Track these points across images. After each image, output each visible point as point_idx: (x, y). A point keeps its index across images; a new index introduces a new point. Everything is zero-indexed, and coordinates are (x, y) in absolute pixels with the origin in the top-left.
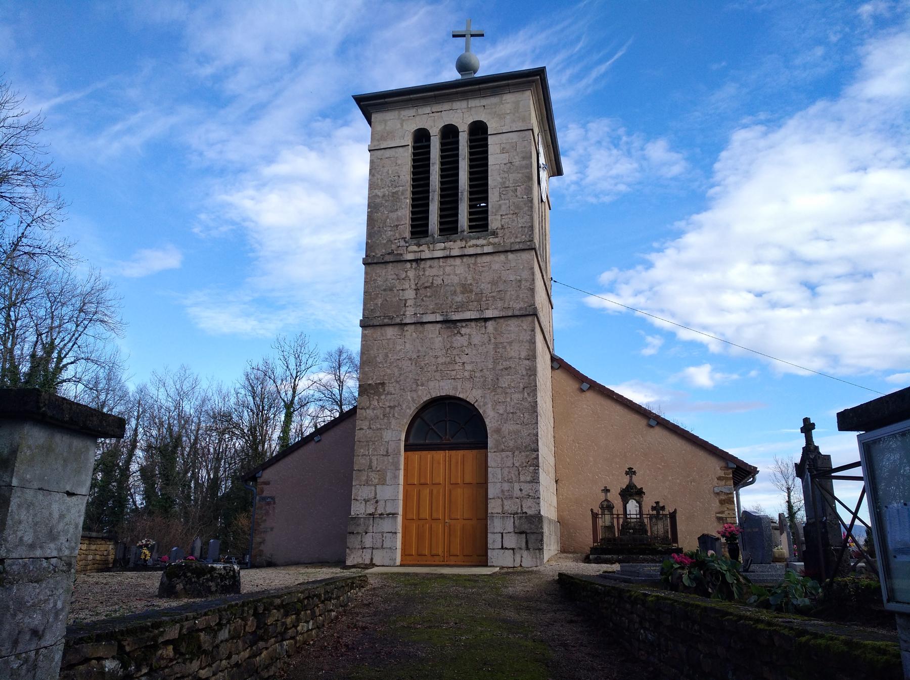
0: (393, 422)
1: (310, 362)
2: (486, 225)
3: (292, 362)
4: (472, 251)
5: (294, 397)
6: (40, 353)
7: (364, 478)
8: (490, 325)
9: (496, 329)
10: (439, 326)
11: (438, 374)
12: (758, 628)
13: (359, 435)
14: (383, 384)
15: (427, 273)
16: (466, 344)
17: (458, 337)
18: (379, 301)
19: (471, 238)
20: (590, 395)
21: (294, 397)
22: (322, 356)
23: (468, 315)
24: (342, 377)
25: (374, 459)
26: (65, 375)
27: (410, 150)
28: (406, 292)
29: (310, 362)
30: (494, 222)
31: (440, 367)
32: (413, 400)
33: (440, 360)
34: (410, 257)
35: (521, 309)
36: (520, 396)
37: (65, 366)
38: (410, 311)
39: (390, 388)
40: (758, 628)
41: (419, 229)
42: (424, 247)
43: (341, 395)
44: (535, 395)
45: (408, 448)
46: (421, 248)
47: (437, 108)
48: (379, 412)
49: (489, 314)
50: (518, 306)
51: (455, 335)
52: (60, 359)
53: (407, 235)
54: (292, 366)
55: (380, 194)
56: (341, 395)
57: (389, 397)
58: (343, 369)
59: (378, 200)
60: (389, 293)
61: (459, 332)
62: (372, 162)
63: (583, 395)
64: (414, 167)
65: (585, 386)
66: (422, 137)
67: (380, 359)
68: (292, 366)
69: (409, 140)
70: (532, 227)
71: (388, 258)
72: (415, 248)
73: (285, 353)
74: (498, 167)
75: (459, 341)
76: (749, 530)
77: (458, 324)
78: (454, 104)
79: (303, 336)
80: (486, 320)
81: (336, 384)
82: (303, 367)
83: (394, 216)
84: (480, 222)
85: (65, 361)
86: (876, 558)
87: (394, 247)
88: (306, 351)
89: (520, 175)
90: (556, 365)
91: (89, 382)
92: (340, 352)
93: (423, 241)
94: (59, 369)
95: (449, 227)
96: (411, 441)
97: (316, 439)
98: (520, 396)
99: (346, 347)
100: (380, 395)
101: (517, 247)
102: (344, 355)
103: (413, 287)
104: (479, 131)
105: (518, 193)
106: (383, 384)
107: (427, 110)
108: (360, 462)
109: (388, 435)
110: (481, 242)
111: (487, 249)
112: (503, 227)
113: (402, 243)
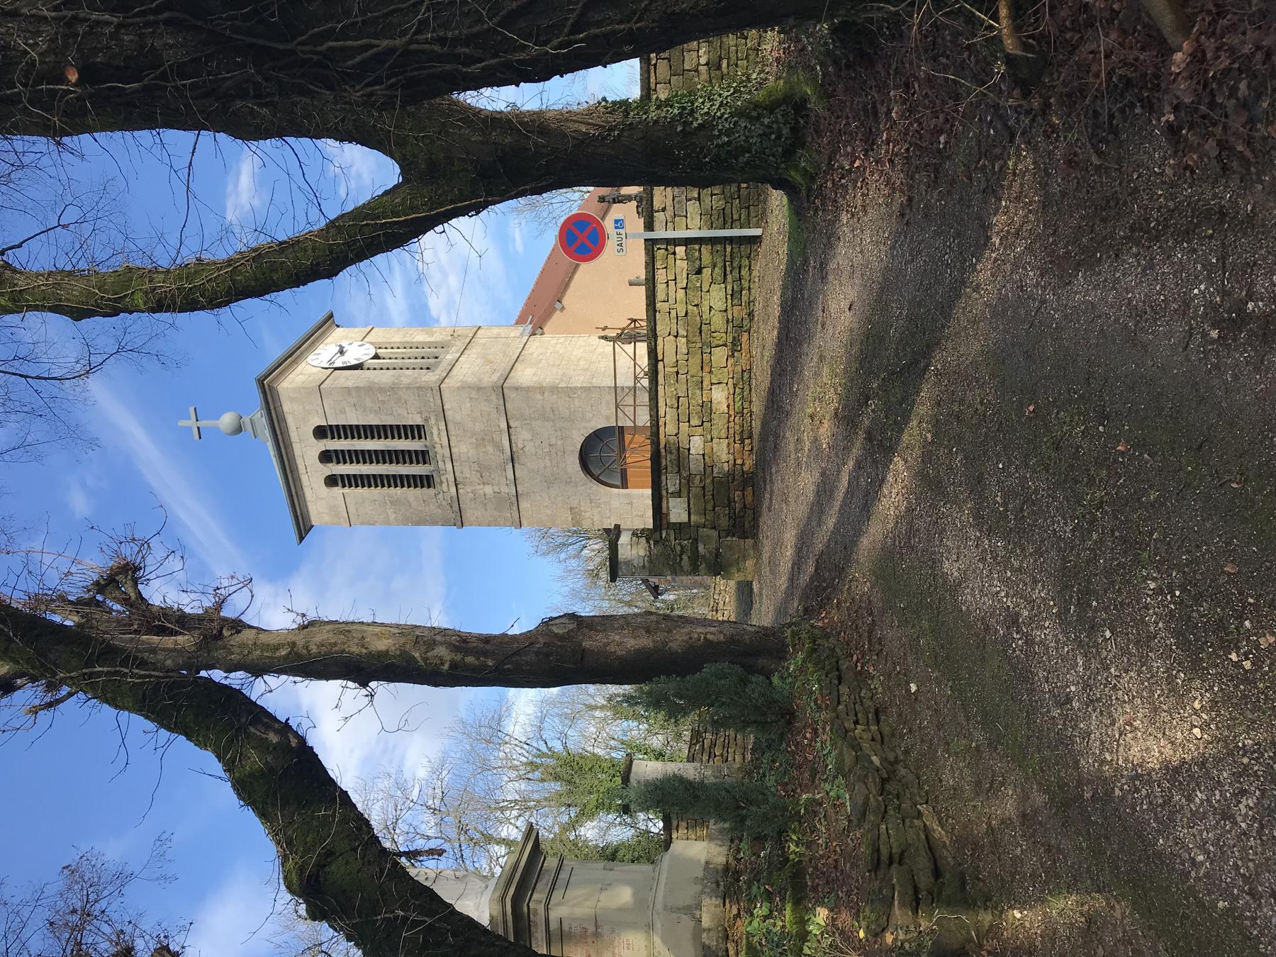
14: (571, 509)
46: (444, 480)
53: (431, 491)
65: (558, 305)
69: (338, 491)
72: (444, 485)
107: (304, 478)
113: (441, 496)
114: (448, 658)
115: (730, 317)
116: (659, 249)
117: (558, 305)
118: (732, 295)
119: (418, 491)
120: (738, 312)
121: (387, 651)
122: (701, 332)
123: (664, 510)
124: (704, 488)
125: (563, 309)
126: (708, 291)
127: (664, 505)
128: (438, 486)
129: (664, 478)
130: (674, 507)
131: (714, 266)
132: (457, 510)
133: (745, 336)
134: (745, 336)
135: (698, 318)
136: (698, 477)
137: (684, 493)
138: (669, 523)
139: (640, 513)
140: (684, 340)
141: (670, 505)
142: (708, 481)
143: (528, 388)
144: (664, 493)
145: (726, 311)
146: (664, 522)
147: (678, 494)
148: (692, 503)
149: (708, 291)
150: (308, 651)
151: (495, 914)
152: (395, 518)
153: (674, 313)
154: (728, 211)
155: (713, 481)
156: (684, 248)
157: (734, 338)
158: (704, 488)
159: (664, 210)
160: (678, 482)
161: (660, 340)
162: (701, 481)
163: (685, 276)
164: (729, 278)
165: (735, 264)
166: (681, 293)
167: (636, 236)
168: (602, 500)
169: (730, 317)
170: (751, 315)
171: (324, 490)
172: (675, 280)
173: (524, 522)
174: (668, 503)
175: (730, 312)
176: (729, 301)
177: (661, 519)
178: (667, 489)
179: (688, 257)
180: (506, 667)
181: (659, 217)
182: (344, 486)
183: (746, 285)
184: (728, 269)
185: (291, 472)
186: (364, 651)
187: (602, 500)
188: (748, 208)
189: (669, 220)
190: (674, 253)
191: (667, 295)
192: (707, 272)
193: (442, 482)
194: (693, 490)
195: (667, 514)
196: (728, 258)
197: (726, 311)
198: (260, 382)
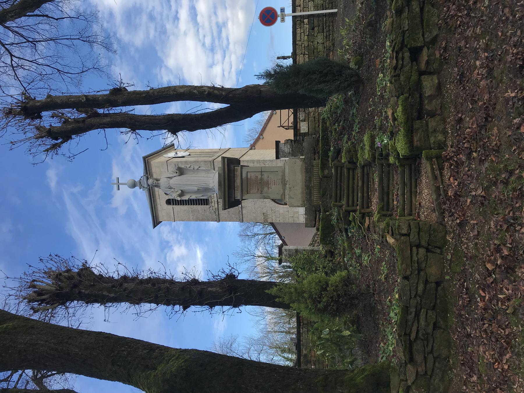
0: (277, 209)
1: (246, 250)
3: (246, 258)
5: (263, 257)
7: (296, 219)
13: (281, 221)
14: (264, 214)
18: (233, 216)
20: (265, 135)
21: (263, 257)
22: (243, 244)
24: (253, 234)
25: (289, 216)
27: (174, 206)
29: (246, 250)
32: (269, 203)
39: (265, 211)
43: (262, 234)
44: (267, 160)
46: (213, 201)
47: (157, 197)
53: (208, 206)
54: (249, 258)
56: (262, 234)
57: (268, 211)
58: (249, 234)
59: (195, 218)
60: (230, 213)
62: (179, 220)
63: (264, 138)
64: (181, 205)
65: (261, 137)
67: (254, 215)
68: (249, 258)
69: (171, 207)
70: (205, 161)
71: (217, 213)
72: (213, 204)
73: (242, 261)
79: (234, 254)
81: (257, 237)
82: (249, 253)
87: (213, 211)
88: (241, 251)
90: (253, 148)
92: (240, 235)
93: (210, 201)
97: (283, 238)
99: (238, 233)
100: (267, 215)
101: (213, 167)
102: (242, 233)
106: (264, 214)
107: (158, 200)
108: (291, 221)
109: (281, 211)
113: (211, 208)
114: (207, 90)
115: (325, 46)
116: (298, 21)
117: (261, 137)
118: (326, 37)
119: (203, 206)
120: (328, 44)
121: (184, 92)
122: (314, 53)
123: (298, 128)
124: (314, 117)
125: (263, 138)
126: (317, 36)
127: (298, 126)
128: (210, 204)
129: (298, 114)
130: (302, 126)
131: (319, 26)
132: (217, 214)
133: (331, 53)
134: (331, 53)
135: (313, 47)
136: (312, 113)
137: (307, 119)
138: (300, 133)
139: (292, 216)
140: (307, 56)
141: (301, 125)
142: (316, 114)
143: (248, 161)
144: (298, 120)
145: (324, 43)
146: (298, 133)
147: (304, 121)
148: (309, 124)
149: (317, 36)
150: (154, 94)
151: (220, 172)
152: (193, 218)
153: (303, 45)
154: (324, 5)
155: (318, 114)
156: (307, 20)
157: (327, 54)
158: (314, 117)
159: (300, 6)
160: (304, 115)
161: (298, 57)
162: (314, 114)
163: (307, 30)
164: (325, 30)
165: (327, 25)
166: (306, 37)
167: (289, 15)
168: (276, 210)
169: (325, 46)
170: (333, 44)
171: (165, 206)
172: (304, 32)
173: (244, 219)
174: (300, 124)
175: (325, 44)
176: (325, 39)
177: (297, 132)
178: (300, 119)
179: (309, 23)
180: (230, 95)
181: (298, 8)
182: (173, 205)
183: (331, 33)
184: (324, 27)
185: (153, 198)
186: (175, 93)
187: (276, 210)
188: (332, 3)
189: (302, 9)
190: (304, 22)
191: (301, 38)
192: (316, 29)
193: (212, 202)
194: (310, 119)
195: (300, 130)
196: (324, 23)
197: (324, 43)
198: (145, 158)
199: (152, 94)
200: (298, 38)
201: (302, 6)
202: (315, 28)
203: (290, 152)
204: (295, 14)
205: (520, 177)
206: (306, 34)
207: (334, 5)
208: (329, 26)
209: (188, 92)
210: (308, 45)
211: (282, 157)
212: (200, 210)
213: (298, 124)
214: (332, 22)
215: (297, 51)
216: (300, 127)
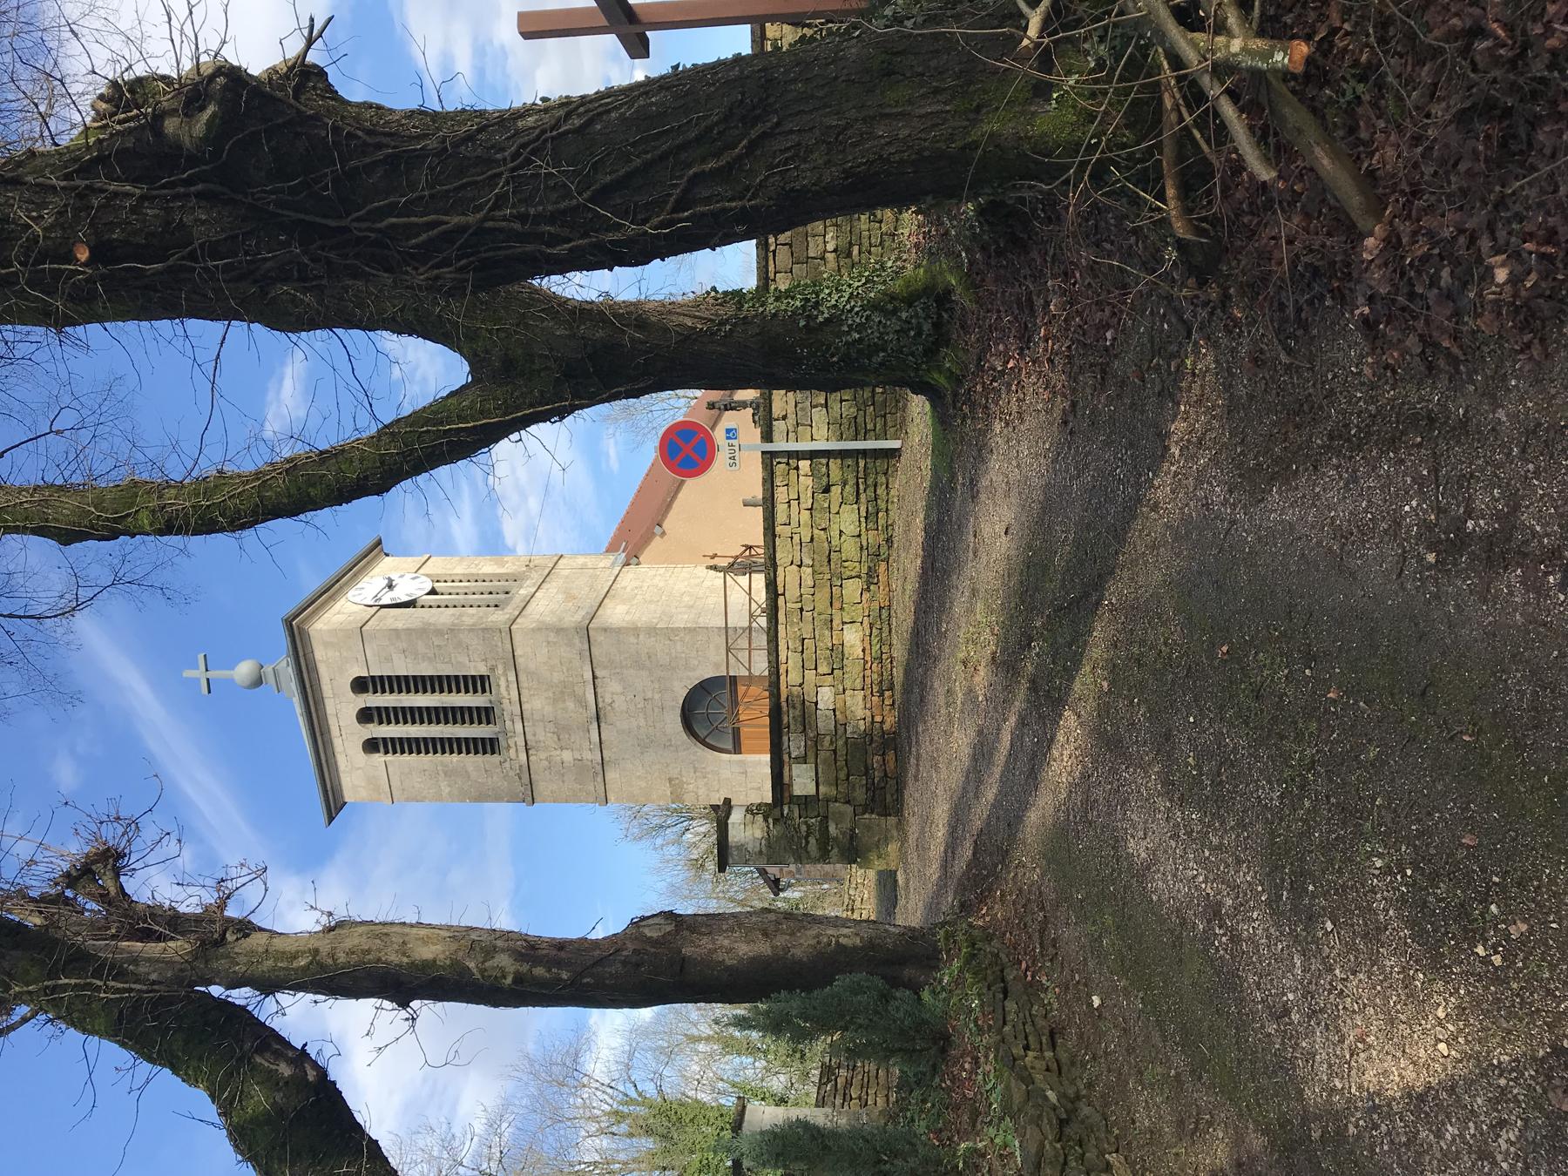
2: (482, 677)
4: (514, 694)
6: (623, 1128)
8: (598, 673)
9: (605, 668)
10: (602, 725)
11: (657, 725)
12: (1274, 174)
14: (670, 780)
15: (542, 739)
16: (623, 698)
17: (616, 705)
19: (499, 693)
23: (591, 698)
25: (749, 786)
26: (650, 1090)
28: (565, 759)
30: (479, 669)
31: (650, 723)
33: (642, 723)
34: (523, 757)
35: (582, 643)
36: (679, 644)
37: (640, 1095)
38: (588, 755)
40: (1274, 174)
41: (488, 746)
42: (511, 742)
45: (737, 749)
46: (512, 745)
48: (701, 783)
49: (589, 676)
50: (579, 643)
51: (613, 709)
52: (632, 1102)
53: (496, 758)
55: (448, 790)
61: (610, 705)
65: (657, 530)
66: (371, 746)
67: (643, 784)
69: (379, 758)
72: (512, 751)
74: (410, 665)
75: (620, 704)
76: (1414, 503)
77: (600, 705)
78: (328, 712)
80: (594, 677)
83: (474, 775)
84: (478, 683)
85: (633, 1094)
86: (901, 429)
87: (512, 773)
89: (420, 642)
91: (658, 1062)
93: (503, 743)
94: (644, 1100)
95: (485, 715)
96: (730, 746)
98: (679, 644)
103: (558, 752)
104: (360, 685)
105: (442, 643)
107: (337, 743)
110: (503, 683)
111: (512, 678)
112: (485, 660)
113: (507, 765)
114: (512, 969)
115: (865, 544)
116: (779, 463)
117: (657, 530)
118: (866, 518)
120: (872, 538)
121: (434, 961)
122: (829, 561)
123: (786, 780)
124: (835, 751)
125: (664, 534)
129: (785, 738)
130: (798, 776)
131: (845, 483)
132: (528, 782)
133: (883, 566)
134: (883, 566)
135: (826, 544)
136: (828, 738)
137: (811, 758)
138: (791, 797)
139: (755, 785)
140: (809, 570)
141: (794, 773)
142: (840, 743)
144: (786, 757)
145: (859, 536)
147: (803, 759)
153: (796, 538)
157: (869, 568)
158: (835, 751)
159: (784, 418)
160: (803, 744)
161: (780, 570)
162: (832, 743)
163: (810, 494)
164: (863, 497)
165: (870, 482)
166: (805, 515)
169: (865, 544)
170: (889, 541)
173: (611, 797)
174: (790, 770)
175: (864, 537)
176: (864, 525)
178: (789, 754)
180: (585, 980)
181: (779, 426)
184: (862, 487)
186: (405, 960)
190: (797, 468)
192: (836, 490)
194: (822, 755)
195: (790, 785)
196: (861, 475)
197: (859, 536)
198: (288, 623)
199: (330, 961)
200: (781, 516)
201: (791, 420)
202: (833, 488)
203: (761, 852)
204: (769, 447)
205: (1346, 12)
206: (803, 506)
207: (890, 424)
208: (875, 486)
209: (448, 962)
210: (812, 539)
211: (736, 863)
212: (470, 769)
213: (786, 769)
214: (885, 474)
215: (778, 556)
216: (791, 777)
